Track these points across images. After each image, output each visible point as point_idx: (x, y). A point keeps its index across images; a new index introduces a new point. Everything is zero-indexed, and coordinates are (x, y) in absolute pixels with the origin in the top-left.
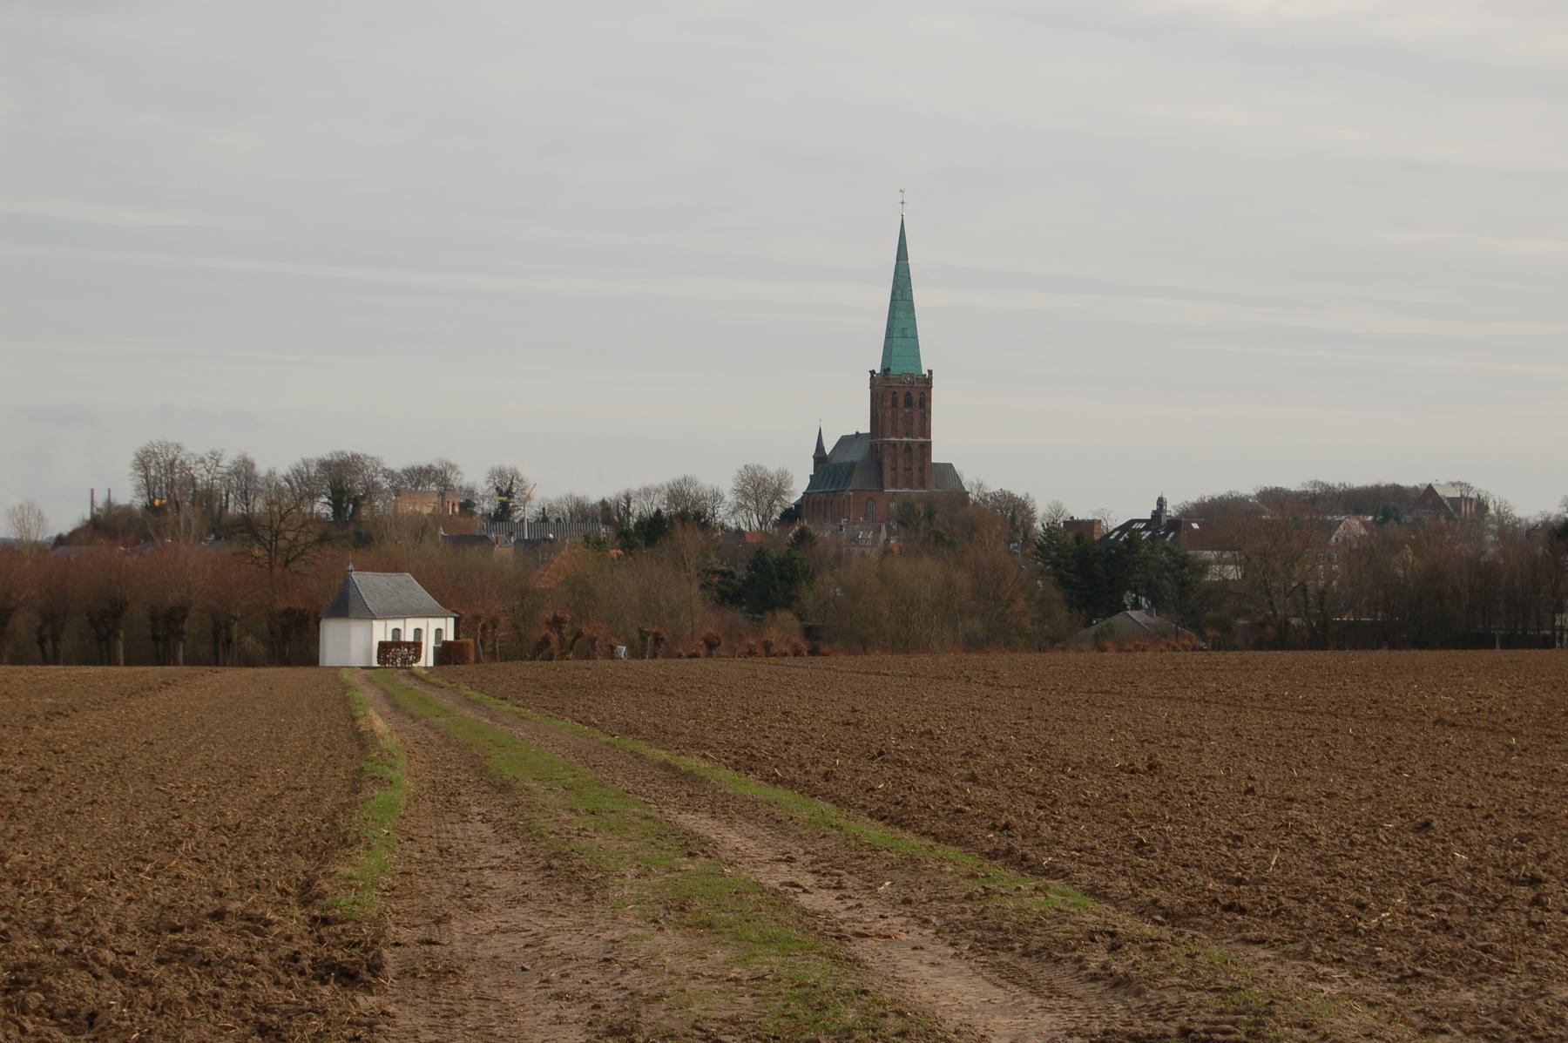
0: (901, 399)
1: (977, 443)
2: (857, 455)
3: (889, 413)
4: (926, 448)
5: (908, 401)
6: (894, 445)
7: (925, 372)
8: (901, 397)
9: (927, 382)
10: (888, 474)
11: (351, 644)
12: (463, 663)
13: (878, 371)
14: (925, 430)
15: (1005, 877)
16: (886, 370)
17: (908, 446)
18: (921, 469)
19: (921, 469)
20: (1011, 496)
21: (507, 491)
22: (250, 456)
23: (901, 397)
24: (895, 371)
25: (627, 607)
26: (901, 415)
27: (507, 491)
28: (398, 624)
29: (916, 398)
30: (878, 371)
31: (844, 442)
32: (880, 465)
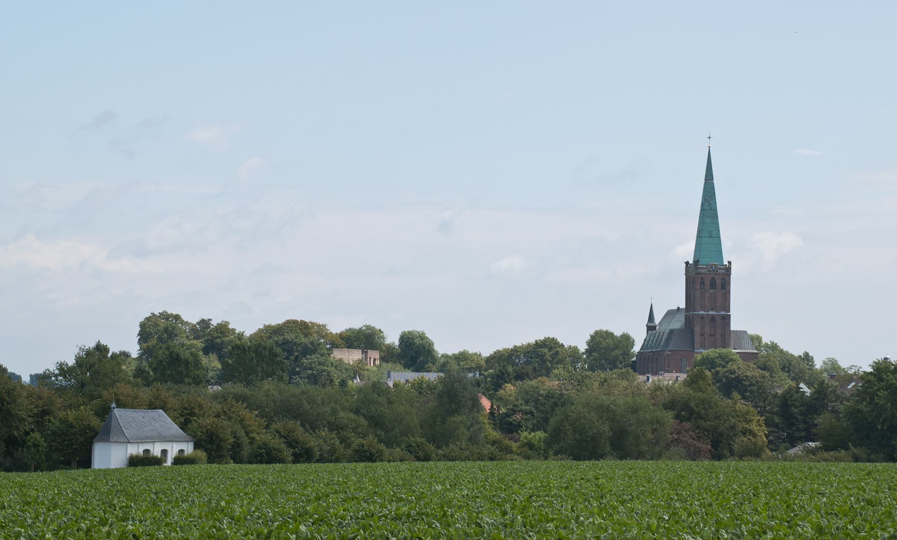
0: (708, 283)
2: (678, 323)
3: (698, 294)
4: (726, 319)
5: (713, 285)
6: (702, 317)
7: (726, 263)
8: (708, 281)
9: (728, 269)
10: (697, 339)
11: (110, 456)
13: (691, 262)
14: (728, 309)
16: (696, 262)
17: (713, 319)
20: (431, 344)
22: (103, 342)
23: (708, 281)
24: (703, 262)
25: (543, 407)
26: (707, 295)
28: (149, 447)
29: (719, 282)
30: (691, 262)
31: (670, 314)
32: (692, 332)
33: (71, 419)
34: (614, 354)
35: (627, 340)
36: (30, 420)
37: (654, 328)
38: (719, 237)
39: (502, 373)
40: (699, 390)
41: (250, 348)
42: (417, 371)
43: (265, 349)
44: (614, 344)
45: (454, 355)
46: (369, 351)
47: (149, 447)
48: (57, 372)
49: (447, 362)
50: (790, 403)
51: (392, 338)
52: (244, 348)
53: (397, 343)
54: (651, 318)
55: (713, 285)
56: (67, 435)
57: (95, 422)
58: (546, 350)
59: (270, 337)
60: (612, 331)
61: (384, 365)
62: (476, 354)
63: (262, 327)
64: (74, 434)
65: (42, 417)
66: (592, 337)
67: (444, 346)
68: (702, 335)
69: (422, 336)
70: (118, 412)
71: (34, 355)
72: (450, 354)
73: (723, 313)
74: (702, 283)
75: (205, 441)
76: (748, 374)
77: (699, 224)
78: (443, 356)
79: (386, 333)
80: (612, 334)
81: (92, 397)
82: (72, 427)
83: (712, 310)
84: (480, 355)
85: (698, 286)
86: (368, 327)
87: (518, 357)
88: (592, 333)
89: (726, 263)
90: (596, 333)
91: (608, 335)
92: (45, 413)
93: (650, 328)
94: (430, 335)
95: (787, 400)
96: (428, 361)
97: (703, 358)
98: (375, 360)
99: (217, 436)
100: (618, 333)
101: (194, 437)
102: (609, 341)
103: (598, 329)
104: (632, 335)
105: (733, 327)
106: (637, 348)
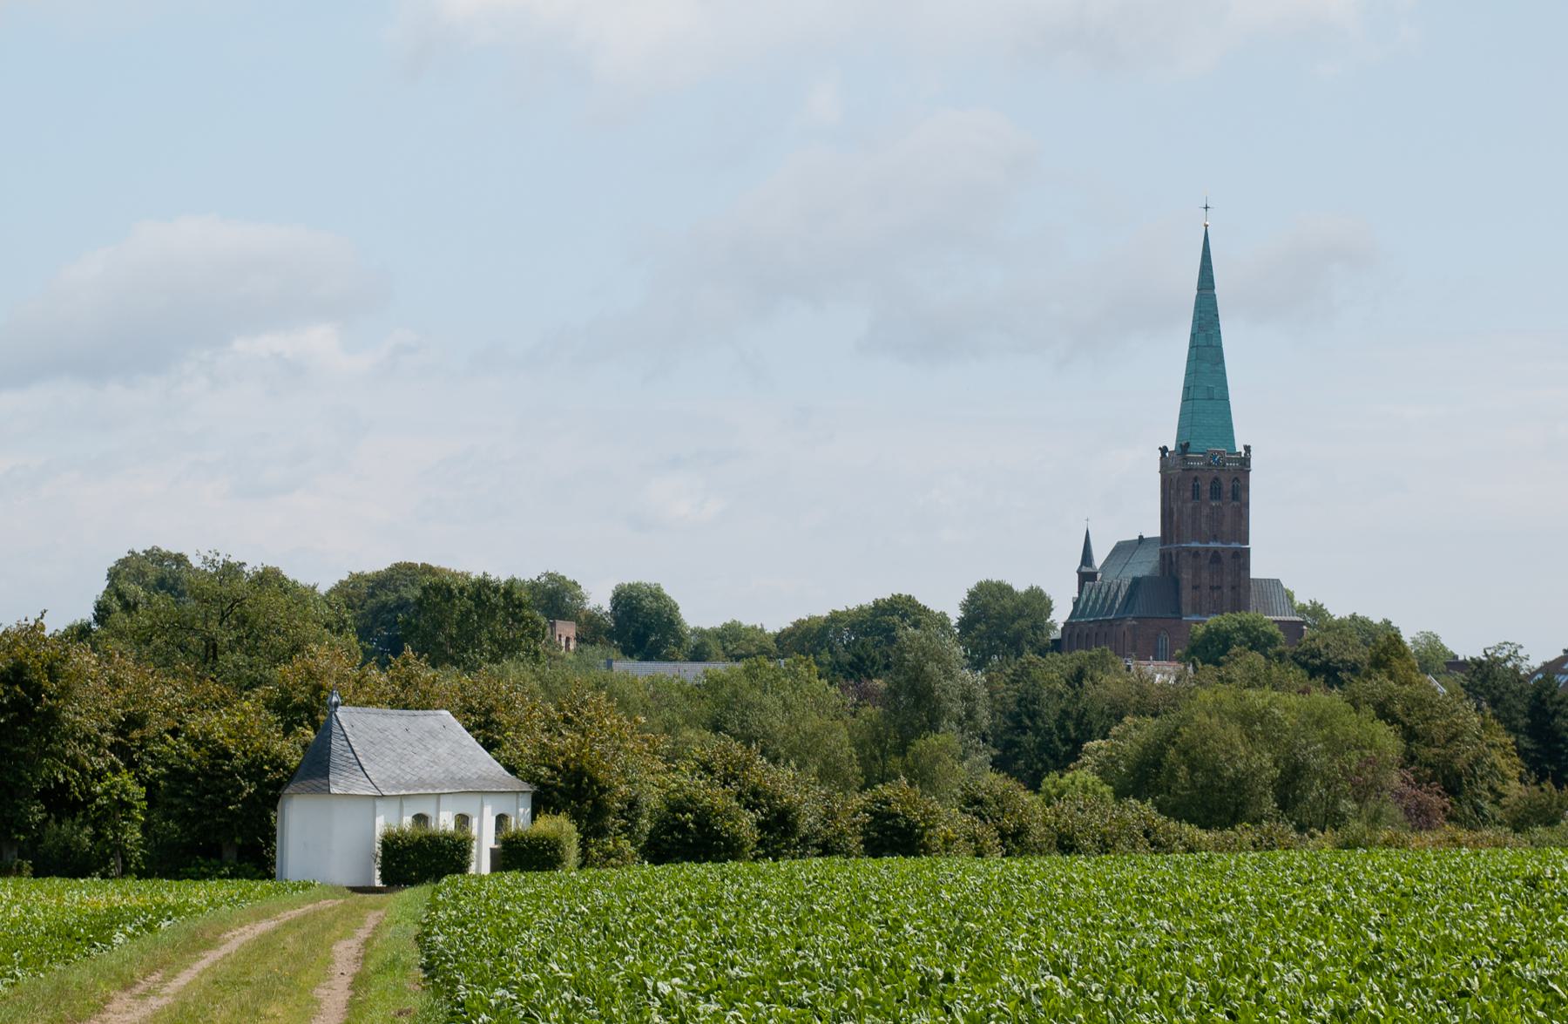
0: (1206, 487)
1: (1302, 553)
2: (1145, 566)
4: (1242, 557)
5: (1216, 492)
6: (1196, 554)
8: (1206, 485)
9: (1244, 463)
10: (1187, 595)
13: (1172, 447)
16: (1183, 448)
17: (1216, 557)
20: (674, 609)
23: (1206, 485)
25: (930, 724)
26: (1205, 511)
29: (1227, 487)
30: (1172, 447)
31: (1123, 550)
32: (1176, 583)
33: (219, 733)
34: (1016, 626)
35: (1037, 602)
38: (1227, 399)
39: (860, 659)
40: (1164, 698)
42: (647, 658)
43: (496, 590)
44: (1016, 607)
45: (714, 630)
46: (559, 623)
47: (426, 808)
49: (704, 644)
50: (1551, 709)
51: (599, 599)
52: (450, 591)
53: (607, 607)
55: (1216, 492)
57: (289, 749)
58: (896, 619)
59: (372, 595)
60: (1008, 582)
61: (589, 650)
62: (754, 628)
63: (345, 578)
64: (230, 774)
66: (972, 594)
67: (699, 613)
68: (1195, 588)
69: (657, 595)
70: (345, 716)
72: (706, 627)
73: (1234, 545)
74: (1196, 493)
75: (560, 790)
76: (1348, 657)
78: (694, 632)
79: (586, 588)
80: (1010, 589)
81: (253, 684)
83: (1215, 538)
84: (762, 630)
85: (1188, 494)
86: (551, 577)
87: (838, 632)
88: (972, 585)
89: (1240, 448)
90: (980, 586)
91: (1003, 590)
92: (135, 721)
93: (1085, 577)
95: (1543, 702)
96: (667, 641)
97: (1208, 630)
98: (568, 639)
99: (593, 781)
100: (1020, 587)
101: (531, 778)
102: (1007, 602)
103: (983, 579)
104: (1047, 591)
105: (1255, 573)
106: (1060, 614)
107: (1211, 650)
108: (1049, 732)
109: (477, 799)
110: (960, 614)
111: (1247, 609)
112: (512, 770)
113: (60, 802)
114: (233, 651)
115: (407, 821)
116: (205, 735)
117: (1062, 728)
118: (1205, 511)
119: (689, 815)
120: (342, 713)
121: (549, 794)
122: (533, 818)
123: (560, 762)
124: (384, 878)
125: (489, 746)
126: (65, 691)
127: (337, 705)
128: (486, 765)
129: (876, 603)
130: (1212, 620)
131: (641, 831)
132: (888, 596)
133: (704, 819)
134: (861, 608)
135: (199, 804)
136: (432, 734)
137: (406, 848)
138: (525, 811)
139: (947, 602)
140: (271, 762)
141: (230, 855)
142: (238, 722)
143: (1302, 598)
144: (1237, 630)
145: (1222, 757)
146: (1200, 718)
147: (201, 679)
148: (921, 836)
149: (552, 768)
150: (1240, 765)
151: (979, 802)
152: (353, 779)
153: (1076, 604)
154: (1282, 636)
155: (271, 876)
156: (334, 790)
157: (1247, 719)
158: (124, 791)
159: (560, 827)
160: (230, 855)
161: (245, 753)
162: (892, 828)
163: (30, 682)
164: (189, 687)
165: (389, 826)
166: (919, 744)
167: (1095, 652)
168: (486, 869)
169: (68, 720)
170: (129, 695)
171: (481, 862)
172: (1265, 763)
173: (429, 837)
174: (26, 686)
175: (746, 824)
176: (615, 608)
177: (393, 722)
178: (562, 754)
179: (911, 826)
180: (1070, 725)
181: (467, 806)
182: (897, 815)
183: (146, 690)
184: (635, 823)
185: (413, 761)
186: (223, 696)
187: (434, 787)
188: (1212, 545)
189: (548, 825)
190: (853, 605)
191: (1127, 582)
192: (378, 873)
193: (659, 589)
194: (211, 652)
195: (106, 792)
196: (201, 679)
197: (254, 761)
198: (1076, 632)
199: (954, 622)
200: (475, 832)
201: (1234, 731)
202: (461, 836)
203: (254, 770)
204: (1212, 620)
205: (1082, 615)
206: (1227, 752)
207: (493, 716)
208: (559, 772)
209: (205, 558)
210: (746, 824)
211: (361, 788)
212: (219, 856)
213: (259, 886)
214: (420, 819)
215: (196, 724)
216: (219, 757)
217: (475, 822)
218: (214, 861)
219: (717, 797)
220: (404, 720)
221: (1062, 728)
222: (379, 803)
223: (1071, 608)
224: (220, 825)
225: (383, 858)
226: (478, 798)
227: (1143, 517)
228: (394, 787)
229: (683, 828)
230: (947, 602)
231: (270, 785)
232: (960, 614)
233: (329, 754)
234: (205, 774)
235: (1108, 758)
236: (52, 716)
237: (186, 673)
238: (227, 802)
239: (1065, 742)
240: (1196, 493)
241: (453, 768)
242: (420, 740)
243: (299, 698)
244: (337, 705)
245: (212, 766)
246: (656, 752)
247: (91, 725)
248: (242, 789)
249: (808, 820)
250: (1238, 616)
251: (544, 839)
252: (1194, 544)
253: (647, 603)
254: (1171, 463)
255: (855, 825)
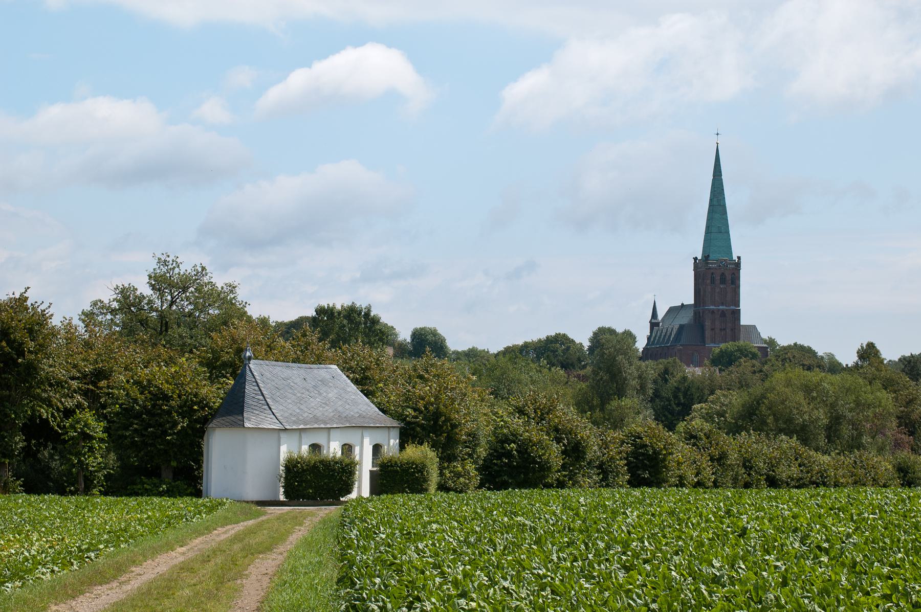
1: (770, 310)
2: (685, 319)
4: (736, 314)
5: (723, 280)
6: (713, 312)
8: (717, 276)
9: (738, 265)
10: (708, 333)
12: (351, 473)
13: (699, 257)
14: (737, 303)
15: (124, 587)
16: (706, 257)
17: (723, 314)
18: (733, 330)
19: (733, 330)
20: (443, 340)
21: (869, 353)
23: (717, 276)
26: (717, 290)
27: (869, 353)
29: (729, 277)
30: (699, 257)
31: (672, 310)
32: (702, 328)
35: (629, 336)
36: (75, 384)
37: (657, 324)
38: (728, 233)
41: (339, 313)
45: (464, 352)
47: (320, 439)
48: (115, 305)
51: (405, 335)
53: (409, 340)
54: (654, 314)
56: (154, 415)
57: (213, 393)
60: (614, 327)
64: (169, 413)
65: (94, 384)
66: (595, 334)
67: (456, 343)
68: (712, 329)
69: (434, 333)
71: (70, 279)
74: (713, 281)
75: (422, 426)
77: (708, 220)
78: (454, 352)
82: (166, 398)
83: (723, 304)
84: (488, 352)
85: (709, 281)
88: (595, 329)
89: (735, 258)
91: (611, 331)
92: (100, 375)
93: (653, 325)
94: (441, 331)
97: (721, 351)
99: (448, 419)
100: (620, 330)
101: (400, 417)
104: (634, 332)
106: (641, 344)
107: (725, 360)
108: (668, 400)
109: (358, 432)
110: (589, 344)
111: (739, 339)
112: (384, 411)
113: (38, 430)
114: (179, 326)
115: (305, 448)
116: (149, 381)
117: (676, 397)
118: (717, 290)
119: (512, 445)
120: (253, 365)
121: (413, 429)
122: (402, 447)
123: (421, 405)
124: (286, 493)
125: (367, 394)
126: (42, 347)
127: (250, 358)
128: (365, 407)
129: (548, 337)
130: (723, 346)
131: (479, 457)
132: (553, 334)
133: (524, 449)
134: (540, 340)
135: (143, 435)
136: (323, 382)
137: (304, 471)
138: (394, 442)
139: (583, 338)
140: (197, 403)
141: (167, 475)
142: (182, 374)
143: (765, 335)
144: (737, 351)
145: (795, 412)
146: (780, 388)
147: (154, 345)
148: (664, 460)
149: (415, 410)
150: (806, 417)
151: (695, 437)
152: (262, 415)
153: (649, 339)
154: (759, 354)
155: (198, 494)
156: (247, 425)
157: (807, 389)
158: (86, 425)
159: (421, 453)
160: (167, 475)
161: (179, 396)
162: (643, 454)
163: (15, 341)
164: (146, 352)
165: (290, 452)
166: (614, 404)
167: (670, 360)
168: (366, 493)
169: (44, 369)
170: (99, 355)
171: (363, 487)
172: (822, 416)
173: (321, 462)
174: (10, 343)
175: (554, 454)
176: (413, 340)
177: (295, 373)
178: (423, 399)
179: (656, 453)
180: (681, 396)
181: (351, 438)
182: (646, 446)
183: (112, 351)
184: (474, 451)
185: (313, 409)
186: (170, 358)
187: (326, 423)
188: (721, 307)
189: (413, 452)
190: (535, 339)
191: (677, 327)
192: (282, 490)
193: (435, 330)
194: (164, 329)
195: (73, 427)
196: (154, 345)
197: (186, 401)
198: (648, 353)
199: (586, 348)
200: (357, 458)
201: (800, 397)
202: (347, 461)
203: (186, 409)
204: (723, 346)
205: (653, 344)
206: (797, 409)
207: (368, 374)
208: (421, 412)
209: (159, 259)
210: (554, 454)
211: (269, 423)
212: (159, 476)
213: (183, 504)
214: (315, 447)
215: (143, 373)
216: (159, 399)
217: (357, 450)
218: (156, 480)
219: (534, 433)
220: (302, 371)
221: (676, 397)
222: (283, 436)
223: (646, 342)
224: (160, 452)
225: (286, 478)
226: (359, 432)
227: (684, 293)
228: (295, 422)
229: (509, 454)
230: (583, 338)
231: (196, 421)
232: (589, 344)
233: (244, 397)
234: (148, 412)
235: (707, 414)
236: (31, 369)
237: (143, 341)
238: (165, 433)
239: (678, 405)
240: (713, 281)
241: (340, 409)
242: (315, 387)
243: (226, 358)
244: (250, 358)
245: (154, 406)
246: (482, 400)
247: (61, 373)
248: (175, 424)
249: (593, 450)
250: (737, 343)
251: (413, 463)
252: (712, 307)
253: (429, 337)
254: (700, 266)
255: (620, 453)
